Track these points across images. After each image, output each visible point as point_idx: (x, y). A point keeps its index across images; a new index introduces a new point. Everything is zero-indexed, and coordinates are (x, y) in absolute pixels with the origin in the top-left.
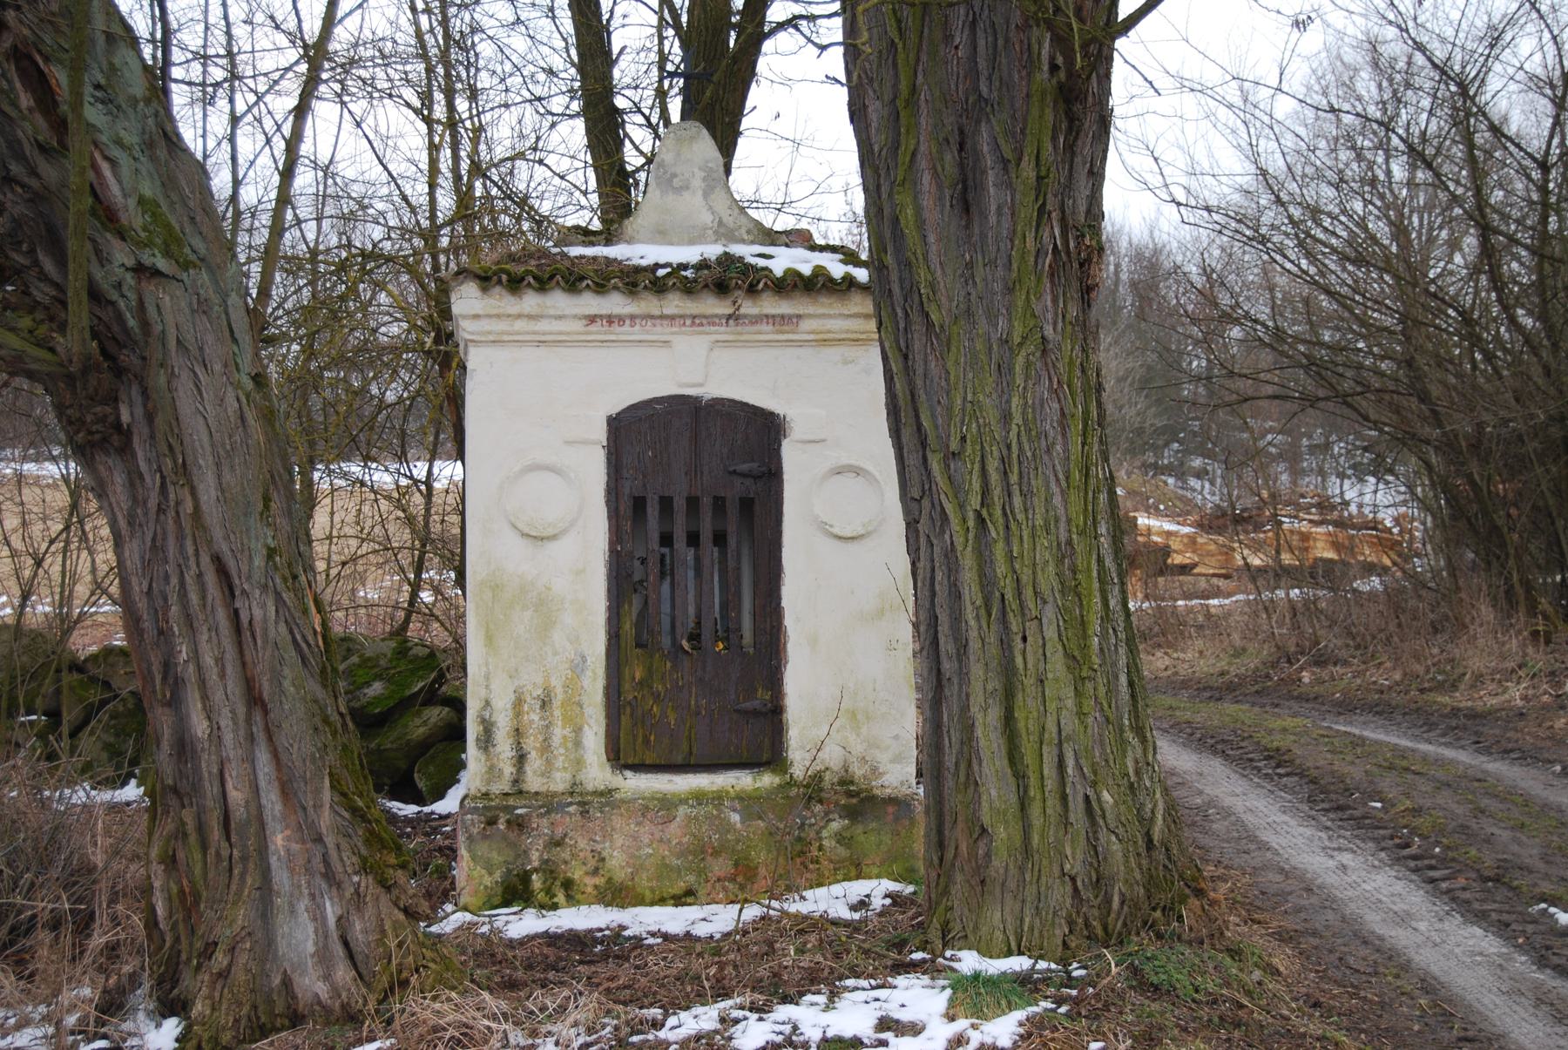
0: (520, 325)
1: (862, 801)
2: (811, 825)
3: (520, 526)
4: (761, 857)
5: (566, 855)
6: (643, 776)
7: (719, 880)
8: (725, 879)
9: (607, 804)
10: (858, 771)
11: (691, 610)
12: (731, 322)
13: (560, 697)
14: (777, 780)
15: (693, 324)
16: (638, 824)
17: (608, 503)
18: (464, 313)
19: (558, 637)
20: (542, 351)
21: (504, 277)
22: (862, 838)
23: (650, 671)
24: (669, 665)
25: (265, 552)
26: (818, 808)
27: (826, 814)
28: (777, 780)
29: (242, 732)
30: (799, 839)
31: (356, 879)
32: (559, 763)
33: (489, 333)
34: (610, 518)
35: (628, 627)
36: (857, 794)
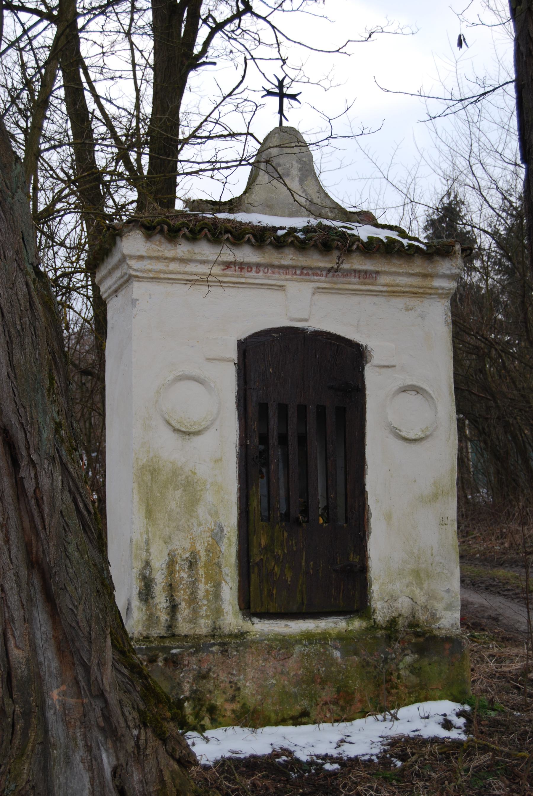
0: (173, 266)
3: (174, 423)
4: (356, 684)
5: (210, 686)
6: (266, 622)
7: (326, 703)
9: (242, 644)
10: (422, 617)
12: (331, 274)
13: (203, 559)
14: (364, 624)
15: (302, 274)
16: (265, 660)
17: (238, 407)
19: (201, 511)
21: (166, 227)
22: (428, 668)
24: (286, 534)
25: (53, 426)
26: (397, 646)
27: (403, 650)
28: (364, 624)
29: (24, 594)
31: (135, 732)
32: (203, 612)
33: (150, 271)
34: (240, 419)
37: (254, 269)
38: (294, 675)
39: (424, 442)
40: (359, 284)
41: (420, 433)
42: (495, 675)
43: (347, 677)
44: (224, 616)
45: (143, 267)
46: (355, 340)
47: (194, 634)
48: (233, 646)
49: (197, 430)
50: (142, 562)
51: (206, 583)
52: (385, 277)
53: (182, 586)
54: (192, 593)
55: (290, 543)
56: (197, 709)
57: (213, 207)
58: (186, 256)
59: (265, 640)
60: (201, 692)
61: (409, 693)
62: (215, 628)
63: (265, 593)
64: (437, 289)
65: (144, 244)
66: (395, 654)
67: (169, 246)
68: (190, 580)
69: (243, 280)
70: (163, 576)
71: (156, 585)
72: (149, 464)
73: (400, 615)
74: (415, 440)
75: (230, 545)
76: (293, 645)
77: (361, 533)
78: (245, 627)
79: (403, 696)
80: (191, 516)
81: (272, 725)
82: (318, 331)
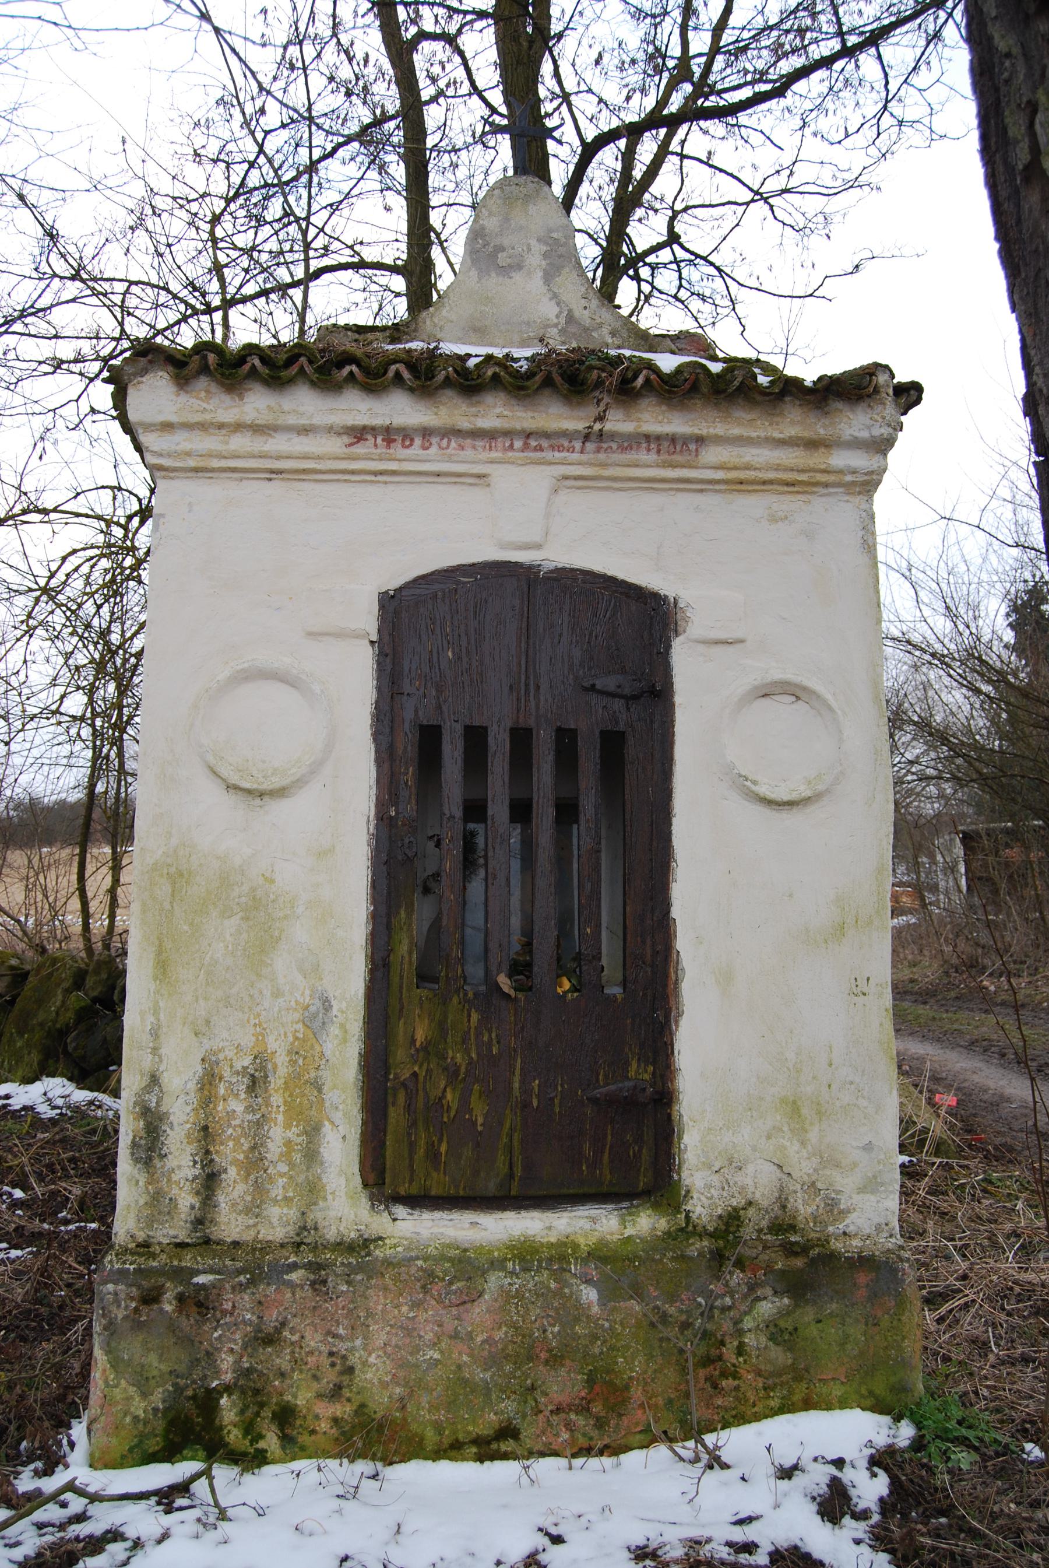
0: (240, 442)
1: (813, 1262)
2: (724, 1309)
3: (224, 772)
4: (633, 1366)
5: (283, 1362)
7: (558, 1410)
8: (570, 1407)
9: (360, 1268)
10: (804, 1208)
11: (516, 922)
12: (589, 446)
13: (283, 1071)
14: (663, 1224)
15: (526, 447)
17: (376, 736)
18: (148, 419)
19: (282, 965)
20: (277, 488)
22: (814, 1330)
23: (442, 1028)
24: (475, 1017)
26: (737, 1278)
27: (752, 1288)
28: (663, 1224)
30: (705, 1335)
32: (277, 1190)
33: (189, 454)
34: (379, 762)
35: (403, 948)
36: (803, 1250)
37: (418, 441)
38: (483, 1342)
39: (810, 809)
40: (658, 466)
41: (802, 788)
42: (1011, 1289)
43: (612, 1348)
44: (325, 1199)
45: (173, 447)
46: (650, 586)
47: (255, 1240)
48: (339, 1271)
49: (277, 786)
50: (142, 1075)
51: (288, 1126)
52: (719, 449)
53: (230, 1131)
54: (254, 1148)
55: (486, 1039)
56: (249, 1413)
57: (357, 336)
58: (265, 418)
59: (417, 1258)
60: (261, 1374)
61: (765, 1389)
62: (304, 1228)
63: (421, 1152)
64: (840, 472)
65: (174, 397)
66: (732, 1297)
67: (227, 399)
68: (250, 1117)
69: (393, 466)
70: (189, 1109)
71: (172, 1129)
72: (169, 861)
73: (750, 1203)
74: (790, 804)
75: (345, 1041)
76: (484, 1273)
77: (659, 1015)
78: (374, 1226)
79: (751, 1396)
80: (259, 975)
81: (426, 1458)
82: (564, 569)
